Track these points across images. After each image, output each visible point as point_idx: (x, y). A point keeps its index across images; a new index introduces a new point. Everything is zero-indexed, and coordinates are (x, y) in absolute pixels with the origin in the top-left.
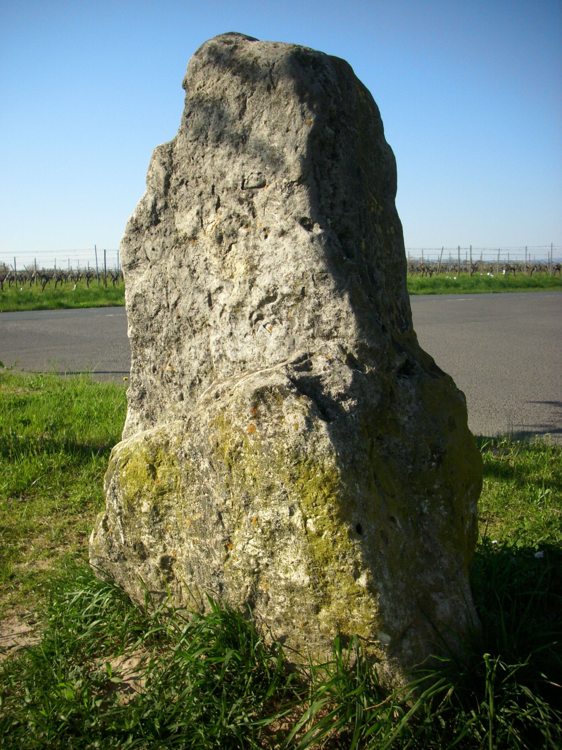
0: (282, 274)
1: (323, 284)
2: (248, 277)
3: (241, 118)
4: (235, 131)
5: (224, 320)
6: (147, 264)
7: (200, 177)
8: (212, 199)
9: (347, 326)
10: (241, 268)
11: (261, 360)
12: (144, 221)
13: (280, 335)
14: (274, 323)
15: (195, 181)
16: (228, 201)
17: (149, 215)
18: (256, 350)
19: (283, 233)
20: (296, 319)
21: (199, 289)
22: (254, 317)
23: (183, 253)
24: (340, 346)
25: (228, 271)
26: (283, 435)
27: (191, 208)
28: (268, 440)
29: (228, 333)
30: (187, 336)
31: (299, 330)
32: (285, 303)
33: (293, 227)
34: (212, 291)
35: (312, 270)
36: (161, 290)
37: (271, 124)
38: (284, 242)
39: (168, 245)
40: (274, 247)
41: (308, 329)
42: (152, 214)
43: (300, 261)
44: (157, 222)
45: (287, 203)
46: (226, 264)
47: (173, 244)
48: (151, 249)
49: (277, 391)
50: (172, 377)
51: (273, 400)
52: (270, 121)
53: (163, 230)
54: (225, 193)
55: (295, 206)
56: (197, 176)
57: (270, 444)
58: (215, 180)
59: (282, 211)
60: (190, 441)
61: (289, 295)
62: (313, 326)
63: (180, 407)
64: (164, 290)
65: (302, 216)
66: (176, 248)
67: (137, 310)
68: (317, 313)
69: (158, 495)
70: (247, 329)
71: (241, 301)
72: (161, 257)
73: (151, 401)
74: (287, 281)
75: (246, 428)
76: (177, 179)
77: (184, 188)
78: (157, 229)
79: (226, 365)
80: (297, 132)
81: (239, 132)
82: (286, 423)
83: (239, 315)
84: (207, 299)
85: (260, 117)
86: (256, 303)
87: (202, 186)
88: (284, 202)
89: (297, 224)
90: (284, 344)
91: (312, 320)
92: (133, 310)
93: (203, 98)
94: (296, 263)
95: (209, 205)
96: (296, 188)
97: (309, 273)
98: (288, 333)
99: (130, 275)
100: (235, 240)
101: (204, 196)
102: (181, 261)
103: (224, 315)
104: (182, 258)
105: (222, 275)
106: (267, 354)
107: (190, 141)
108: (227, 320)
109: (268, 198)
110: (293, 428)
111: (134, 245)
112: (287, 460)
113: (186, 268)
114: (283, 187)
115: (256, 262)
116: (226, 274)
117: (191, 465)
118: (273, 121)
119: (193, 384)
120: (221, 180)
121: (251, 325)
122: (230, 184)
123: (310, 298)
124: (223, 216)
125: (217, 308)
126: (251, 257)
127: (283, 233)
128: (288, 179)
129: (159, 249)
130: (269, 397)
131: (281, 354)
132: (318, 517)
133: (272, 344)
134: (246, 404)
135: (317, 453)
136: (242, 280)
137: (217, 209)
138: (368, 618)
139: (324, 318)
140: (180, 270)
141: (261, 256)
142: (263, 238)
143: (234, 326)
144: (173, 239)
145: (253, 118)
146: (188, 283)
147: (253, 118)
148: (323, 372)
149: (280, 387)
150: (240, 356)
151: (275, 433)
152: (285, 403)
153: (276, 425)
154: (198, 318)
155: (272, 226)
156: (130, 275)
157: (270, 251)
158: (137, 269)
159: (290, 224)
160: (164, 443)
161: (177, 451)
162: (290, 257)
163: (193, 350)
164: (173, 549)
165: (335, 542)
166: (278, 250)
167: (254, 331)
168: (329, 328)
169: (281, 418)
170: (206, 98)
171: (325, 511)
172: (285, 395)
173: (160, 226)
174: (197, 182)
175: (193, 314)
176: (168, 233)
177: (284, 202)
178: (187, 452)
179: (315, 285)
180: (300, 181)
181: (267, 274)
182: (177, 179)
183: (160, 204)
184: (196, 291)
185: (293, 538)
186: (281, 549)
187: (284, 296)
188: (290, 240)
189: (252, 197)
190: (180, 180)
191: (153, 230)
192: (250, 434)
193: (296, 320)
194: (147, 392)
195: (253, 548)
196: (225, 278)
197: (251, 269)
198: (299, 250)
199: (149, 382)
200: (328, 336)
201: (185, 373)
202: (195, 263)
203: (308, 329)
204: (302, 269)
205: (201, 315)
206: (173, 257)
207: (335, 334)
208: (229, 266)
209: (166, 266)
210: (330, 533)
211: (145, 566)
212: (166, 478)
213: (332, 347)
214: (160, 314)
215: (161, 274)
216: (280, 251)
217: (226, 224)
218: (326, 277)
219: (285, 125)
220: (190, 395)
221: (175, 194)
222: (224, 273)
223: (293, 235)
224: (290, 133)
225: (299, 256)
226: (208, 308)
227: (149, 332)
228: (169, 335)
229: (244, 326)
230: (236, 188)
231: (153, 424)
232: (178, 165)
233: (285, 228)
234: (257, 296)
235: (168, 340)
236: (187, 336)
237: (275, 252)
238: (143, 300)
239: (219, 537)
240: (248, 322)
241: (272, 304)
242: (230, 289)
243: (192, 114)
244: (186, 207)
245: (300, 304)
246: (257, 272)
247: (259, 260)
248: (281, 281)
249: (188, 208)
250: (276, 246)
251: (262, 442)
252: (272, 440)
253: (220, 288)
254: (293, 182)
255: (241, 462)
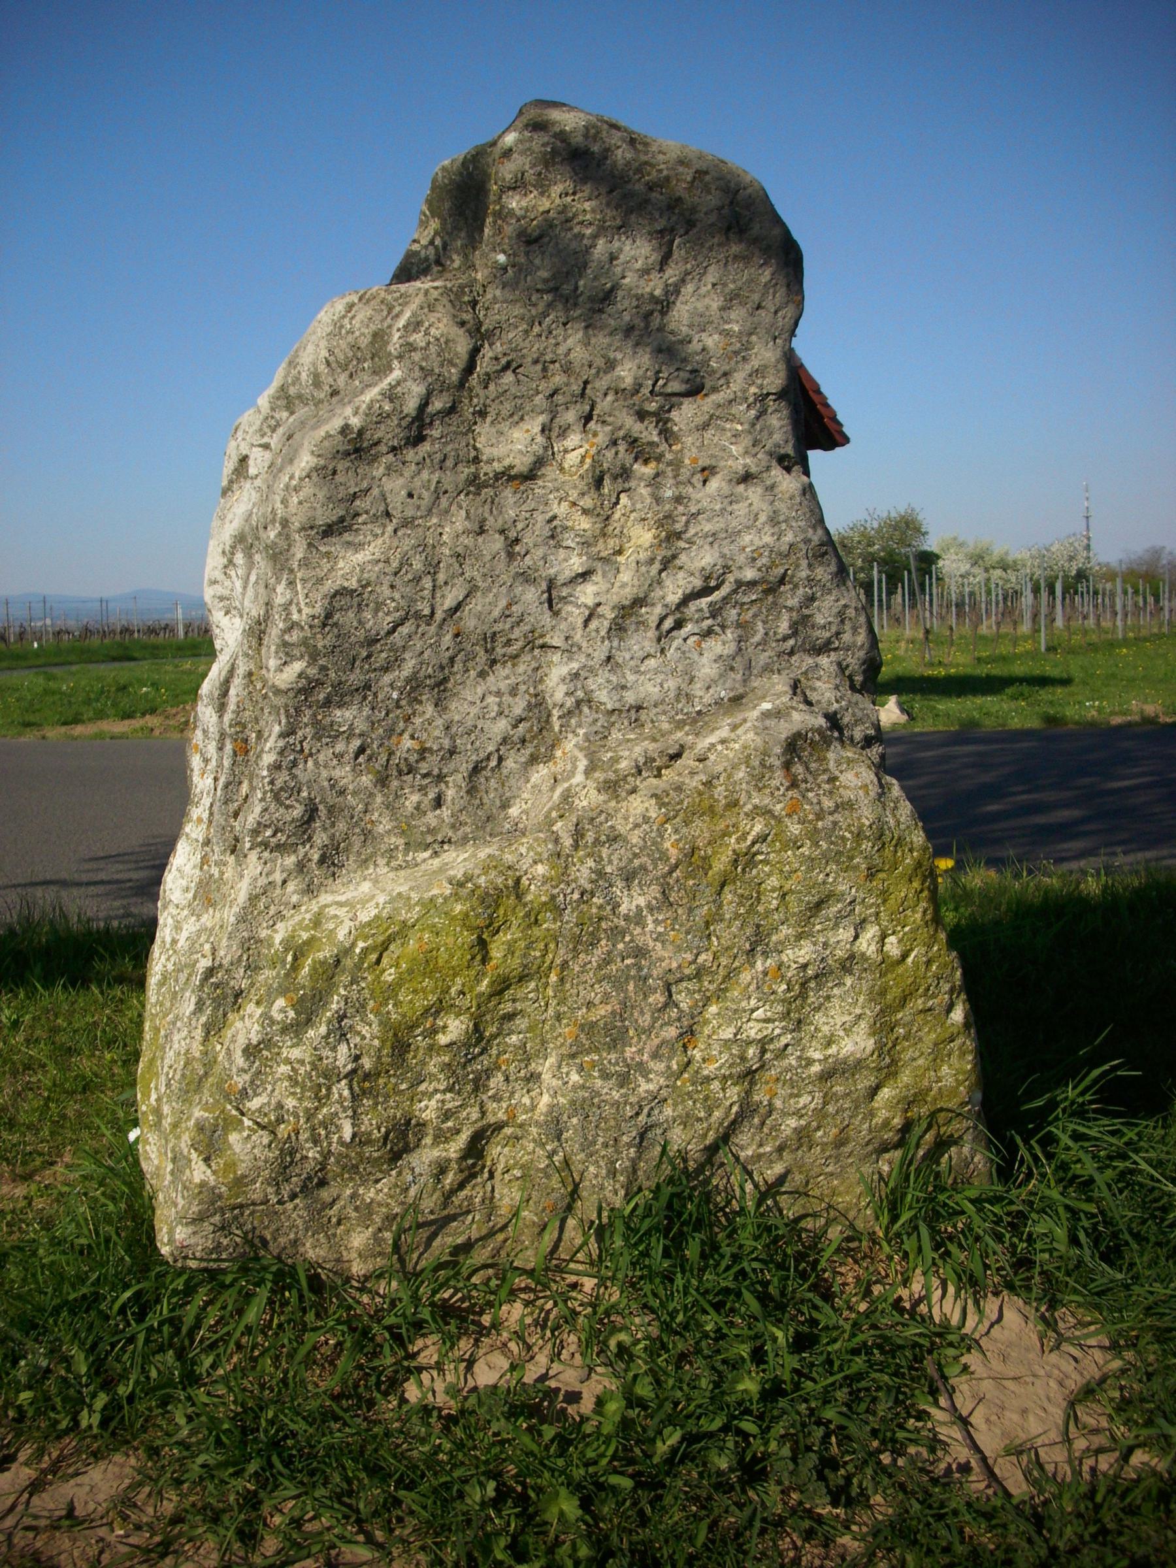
0: (744, 549)
1: (821, 564)
2: (662, 553)
3: (661, 270)
4: (648, 290)
5: (594, 634)
6: (384, 526)
7: (553, 362)
8: (578, 406)
9: (855, 630)
10: (643, 537)
11: (683, 701)
12: (389, 433)
13: (726, 652)
14: (709, 633)
15: (539, 367)
16: (617, 413)
17: (404, 423)
18: (671, 684)
19: (746, 478)
20: (760, 623)
21: (526, 578)
22: (668, 623)
23: (487, 507)
24: (839, 664)
25: (612, 543)
26: (849, 806)
27: (522, 419)
28: (831, 818)
29: (603, 658)
30: (473, 673)
31: (764, 642)
32: (740, 597)
33: (768, 468)
34: (561, 579)
35: (807, 541)
36: (417, 579)
37: (727, 290)
38: (750, 492)
39: (450, 488)
40: (726, 501)
41: (785, 638)
42: (412, 423)
43: (784, 526)
44: (420, 439)
45: (758, 427)
46: (611, 528)
47: (461, 487)
48: (404, 493)
49: (817, 738)
50: (417, 762)
51: (811, 755)
52: (725, 285)
53: (438, 456)
54: (610, 398)
55: (771, 434)
56: (548, 358)
57: (835, 823)
58: (593, 371)
59: (747, 441)
60: (590, 863)
61: (752, 584)
62: (795, 634)
63: (434, 823)
64: (427, 583)
65: (782, 451)
66: (467, 495)
67: (336, 624)
68: (806, 612)
69: (491, 996)
70: (650, 646)
71: (641, 595)
72: (430, 511)
73: (333, 825)
74: (754, 560)
75: (779, 807)
76: (497, 359)
77: (509, 377)
78: (421, 454)
79: (590, 720)
80: (776, 312)
81: (657, 293)
82: (845, 787)
83: (630, 623)
84: (546, 595)
85: (702, 275)
86: (673, 598)
87: (558, 379)
88: (753, 425)
89: (774, 463)
90: (732, 669)
91: (796, 623)
92: (324, 625)
93: (575, 215)
94: (776, 529)
95: (570, 416)
96: (771, 404)
97: (802, 546)
98: (740, 649)
99: (323, 549)
100: (627, 486)
101: (560, 399)
102: (485, 520)
103: (594, 624)
104: (487, 515)
105: (594, 550)
106: (697, 689)
107: (538, 291)
108: (603, 633)
109: (711, 417)
110: (861, 792)
111: (349, 482)
112: (866, 845)
113: (497, 536)
114: (751, 400)
115: (678, 527)
116: (604, 548)
117: (594, 910)
118: (732, 286)
119: (476, 770)
120: (605, 373)
121: (659, 640)
122: (628, 381)
123: (796, 586)
124: (602, 439)
125: (574, 614)
126: (669, 516)
127: (746, 478)
128: (761, 387)
129: (426, 494)
130: (804, 750)
131: (727, 685)
132: (907, 929)
133: (707, 668)
134: (771, 766)
135: (902, 827)
136: (643, 556)
137: (585, 425)
138: (964, 1073)
139: (820, 620)
140: (480, 539)
141: (695, 516)
142: (699, 485)
143: (615, 644)
144: (463, 477)
145: (687, 273)
146: (501, 566)
147: (687, 273)
148: (836, 706)
149: (820, 731)
150: (630, 698)
151: (837, 806)
152: (831, 756)
153: (831, 793)
154: (517, 633)
155: (722, 463)
156: (323, 549)
157: (718, 507)
158: (347, 537)
159: (764, 464)
160: (510, 882)
161: (555, 891)
162: (763, 518)
163: (491, 699)
164: (504, 1105)
165: (929, 963)
166: (735, 506)
167: (662, 651)
168: (828, 635)
169: (833, 780)
170: (581, 218)
171: (918, 916)
172: (827, 742)
173: (426, 447)
174: (545, 369)
175: (508, 626)
176: (449, 463)
177: (753, 425)
178: (588, 887)
179: (810, 566)
180: (781, 395)
181: (707, 547)
182: (497, 359)
183: (437, 405)
184: (521, 579)
185: (849, 981)
186: (817, 1009)
187: (739, 584)
188: (759, 490)
189: (669, 411)
190: (504, 361)
191: (410, 454)
192: (789, 815)
193: (760, 626)
194: (321, 807)
195: (761, 1025)
196: (603, 554)
197: (668, 538)
198: (781, 506)
199: (326, 784)
200: (823, 648)
201: (460, 748)
202: (520, 526)
203: (785, 638)
204: (789, 537)
205: (528, 628)
206: (463, 513)
207: (837, 644)
208: (617, 532)
209: (440, 530)
210: (923, 950)
211: (399, 1174)
212: (517, 954)
213: (826, 667)
214: (404, 630)
215: (422, 546)
216: (741, 509)
217: (610, 454)
218: (826, 553)
219: (756, 297)
220: (468, 792)
221: (486, 387)
222: (601, 545)
223: (768, 483)
224: (762, 312)
225: (782, 518)
226: (548, 614)
227: (358, 671)
228: (422, 674)
229: (640, 642)
230: (638, 392)
231: (334, 874)
232: (497, 332)
233: (753, 470)
234: (673, 589)
235: (414, 686)
236: (473, 673)
237: (729, 509)
238: (355, 603)
239: (672, 1032)
240: (652, 634)
241: (709, 599)
242: (610, 575)
243: (546, 240)
244: (511, 415)
245: (770, 598)
246: (682, 544)
247: (687, 522)
248: (741, 559)
249: (516, 418)
250: (732, 499)
251: (820, 823)
252: (837, 817)
253: (585, 575)
254: (768, 394)
255: (754, 872)
